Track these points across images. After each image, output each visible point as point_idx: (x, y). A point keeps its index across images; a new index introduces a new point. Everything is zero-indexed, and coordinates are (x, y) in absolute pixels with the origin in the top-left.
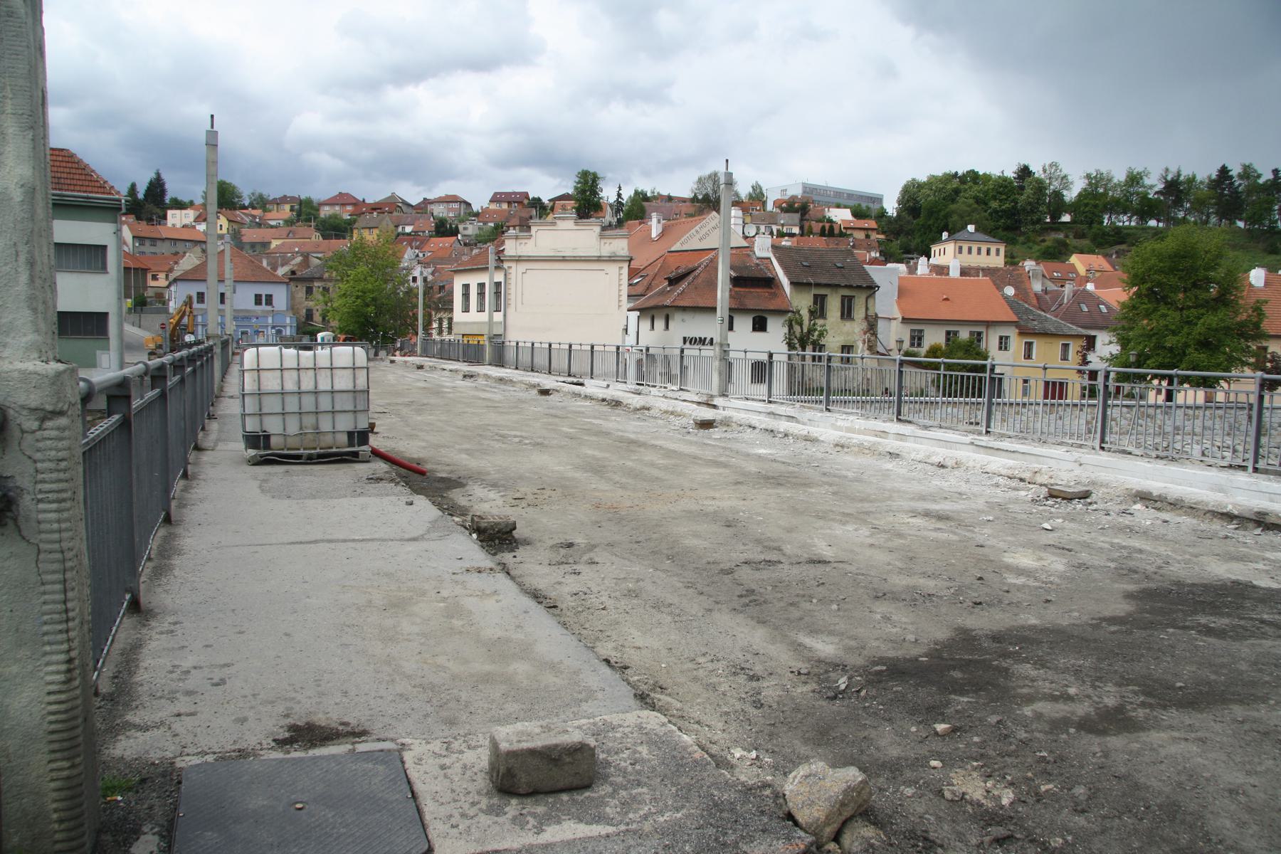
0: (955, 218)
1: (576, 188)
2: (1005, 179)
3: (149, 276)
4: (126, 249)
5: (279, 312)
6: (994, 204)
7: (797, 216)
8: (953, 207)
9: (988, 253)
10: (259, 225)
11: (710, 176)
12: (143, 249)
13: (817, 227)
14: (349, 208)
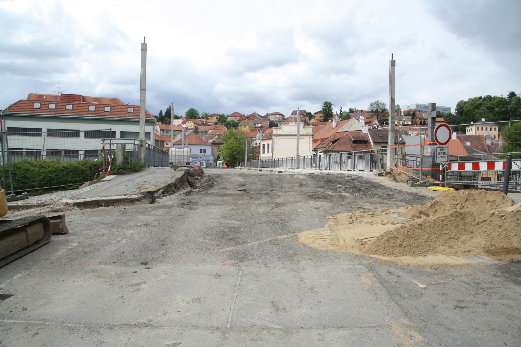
0: (477, 115)
1: (323, 109)
2: (502, 98)
3: (165, 143)
4: (158, 134)
5: (208, 156)
6: (497, 109)
7: (410, 117)
8: (477, 111)
9: (491, 130)
10: (205, 124)
11: (375, 103)
12: (163, 134)
13: (418, 121)
14: (238, 118)
